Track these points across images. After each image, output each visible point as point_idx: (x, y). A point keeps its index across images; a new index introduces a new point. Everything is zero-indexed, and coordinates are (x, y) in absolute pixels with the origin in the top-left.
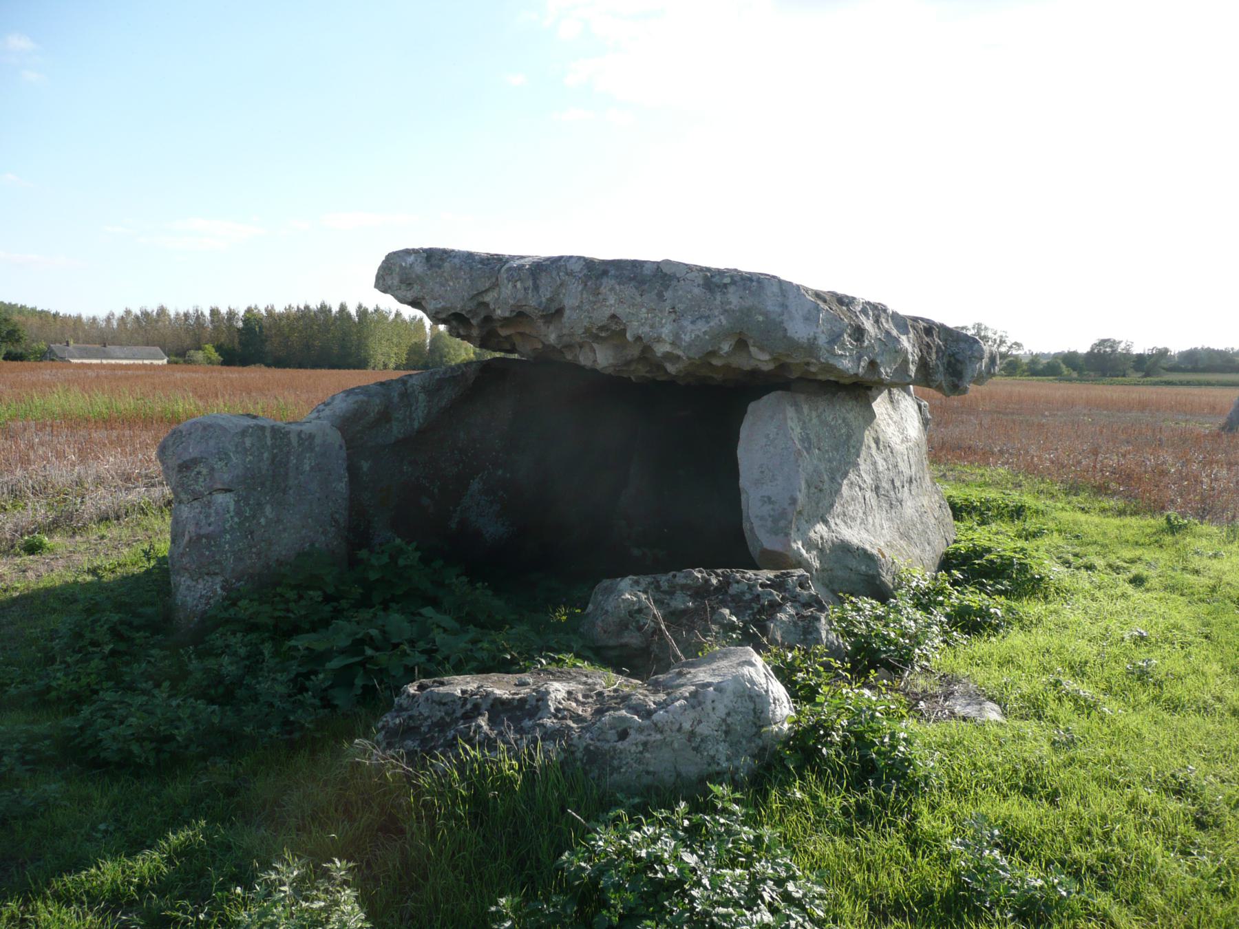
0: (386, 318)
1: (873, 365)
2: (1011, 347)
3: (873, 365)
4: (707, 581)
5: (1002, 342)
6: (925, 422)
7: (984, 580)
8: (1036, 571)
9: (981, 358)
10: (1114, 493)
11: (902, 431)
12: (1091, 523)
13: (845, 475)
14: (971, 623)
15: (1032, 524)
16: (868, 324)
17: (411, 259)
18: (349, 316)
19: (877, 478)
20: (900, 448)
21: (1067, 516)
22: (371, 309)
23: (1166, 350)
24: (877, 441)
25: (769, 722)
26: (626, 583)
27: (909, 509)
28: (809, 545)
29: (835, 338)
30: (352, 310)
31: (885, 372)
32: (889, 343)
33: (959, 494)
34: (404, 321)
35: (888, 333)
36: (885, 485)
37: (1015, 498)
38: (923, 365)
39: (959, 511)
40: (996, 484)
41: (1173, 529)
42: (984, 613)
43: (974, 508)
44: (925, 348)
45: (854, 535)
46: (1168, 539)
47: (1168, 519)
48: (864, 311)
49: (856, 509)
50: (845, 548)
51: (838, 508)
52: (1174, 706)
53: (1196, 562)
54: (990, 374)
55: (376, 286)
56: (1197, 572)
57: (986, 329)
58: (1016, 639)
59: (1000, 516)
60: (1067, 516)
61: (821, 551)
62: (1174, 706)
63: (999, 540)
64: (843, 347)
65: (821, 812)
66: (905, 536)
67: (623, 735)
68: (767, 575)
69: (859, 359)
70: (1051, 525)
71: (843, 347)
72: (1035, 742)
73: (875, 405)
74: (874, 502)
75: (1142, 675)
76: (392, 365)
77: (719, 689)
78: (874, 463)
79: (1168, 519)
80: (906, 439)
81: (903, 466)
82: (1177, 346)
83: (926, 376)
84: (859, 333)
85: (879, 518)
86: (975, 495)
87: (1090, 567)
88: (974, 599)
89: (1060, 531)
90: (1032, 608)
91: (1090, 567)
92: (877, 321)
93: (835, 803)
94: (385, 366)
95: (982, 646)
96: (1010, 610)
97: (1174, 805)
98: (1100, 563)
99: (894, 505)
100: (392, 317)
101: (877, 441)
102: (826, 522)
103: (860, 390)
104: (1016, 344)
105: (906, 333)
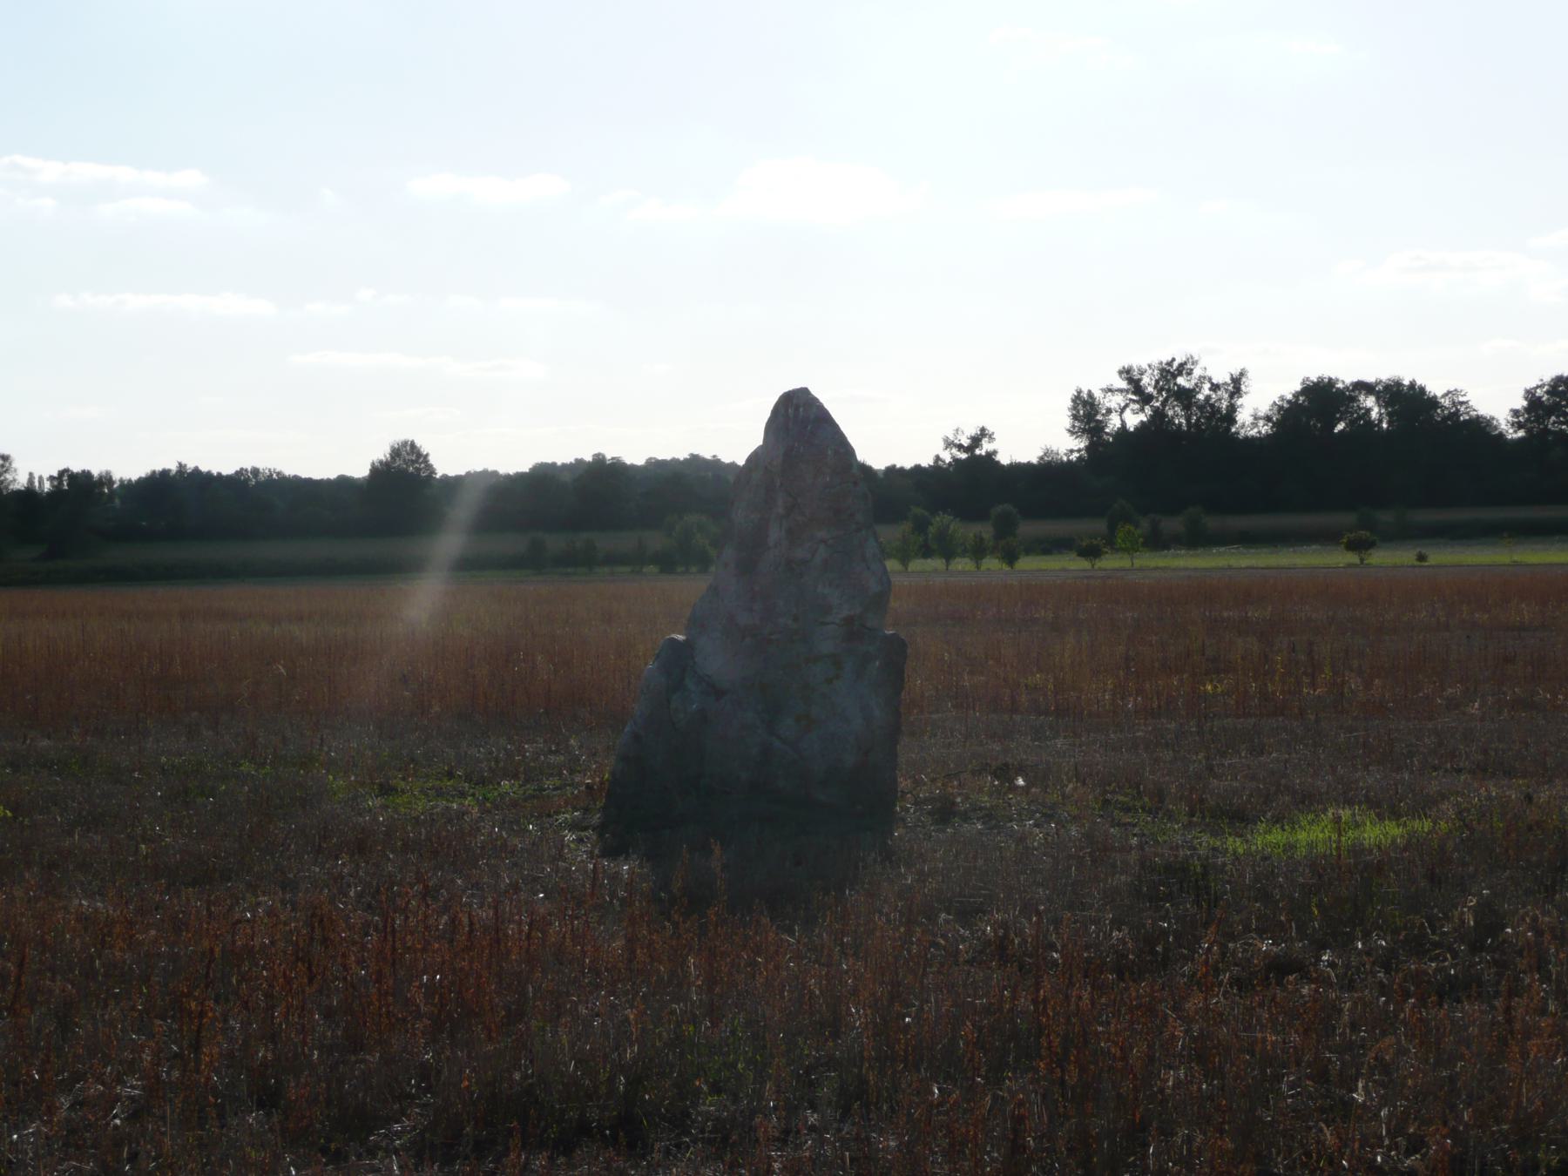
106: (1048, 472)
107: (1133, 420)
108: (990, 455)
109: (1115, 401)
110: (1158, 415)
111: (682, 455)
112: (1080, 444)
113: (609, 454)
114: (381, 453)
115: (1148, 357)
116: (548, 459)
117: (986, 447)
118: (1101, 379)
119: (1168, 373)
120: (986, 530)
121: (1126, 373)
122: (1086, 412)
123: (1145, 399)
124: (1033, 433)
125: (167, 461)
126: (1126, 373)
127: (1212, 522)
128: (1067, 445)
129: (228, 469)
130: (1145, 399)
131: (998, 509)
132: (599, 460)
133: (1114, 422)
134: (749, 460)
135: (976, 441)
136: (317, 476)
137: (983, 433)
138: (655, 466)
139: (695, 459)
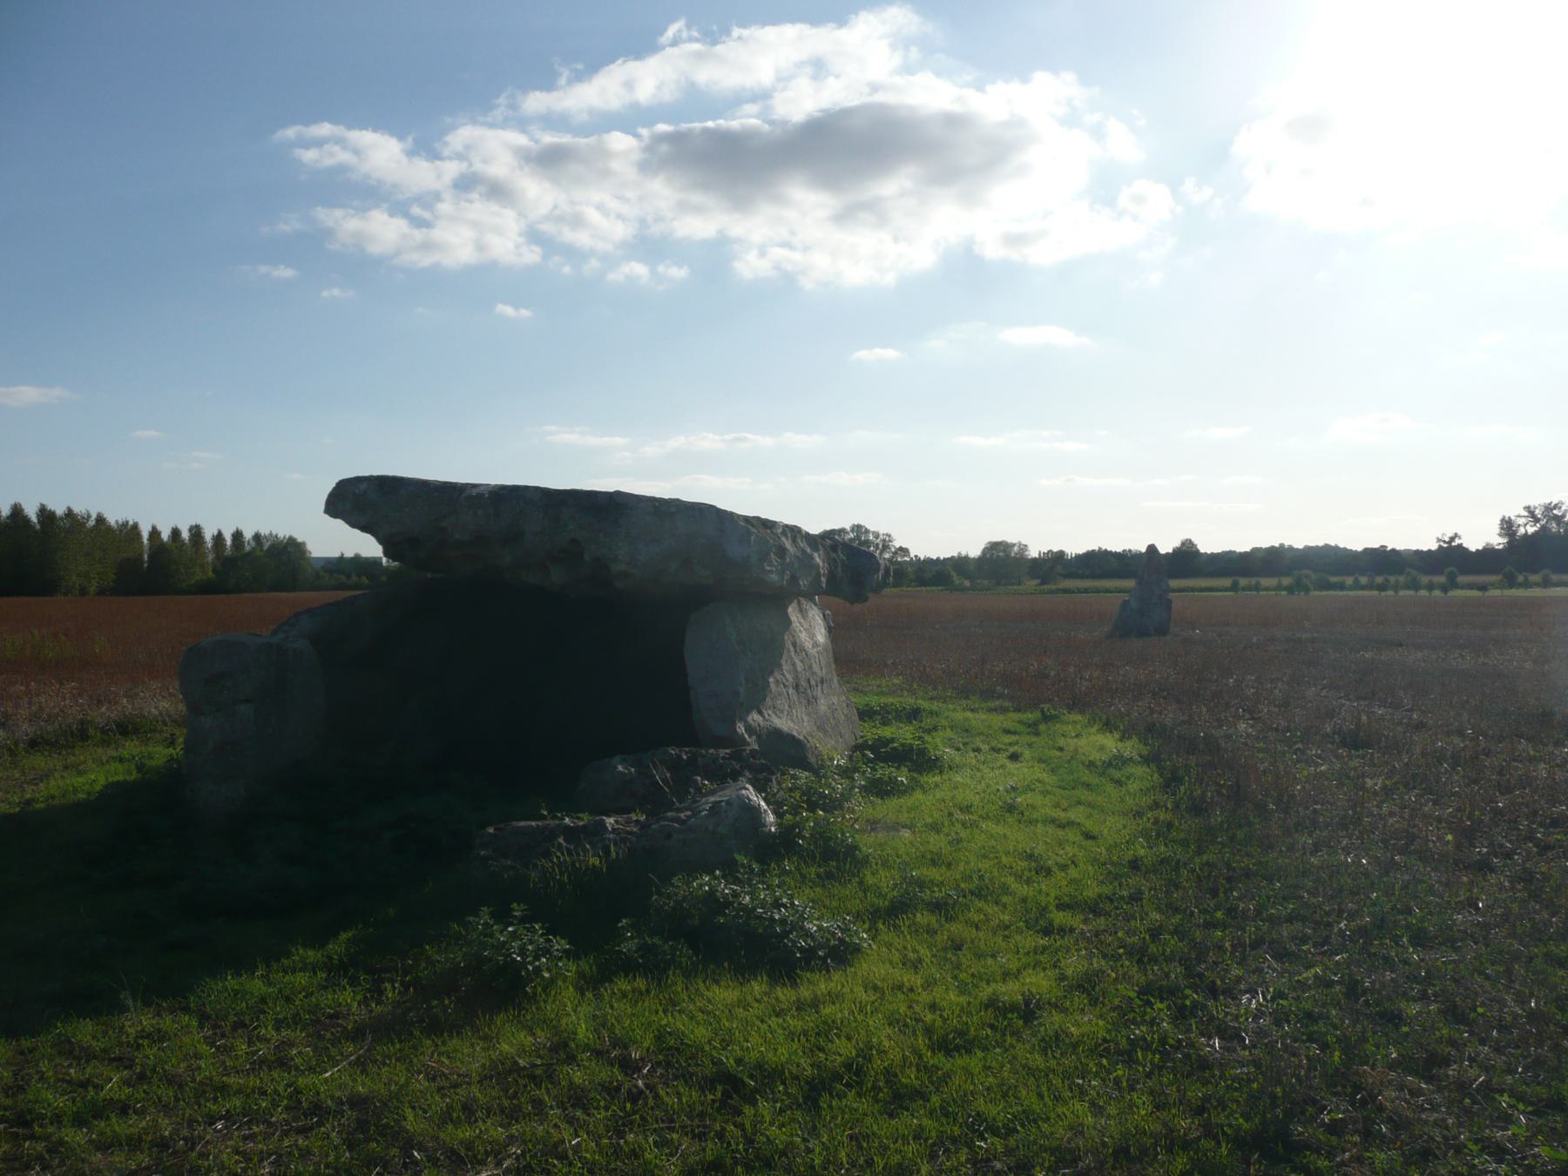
0: (83, 525)
1: (794, 579)
2: (895, 553)
3: (794, 579)
4: (679, 757)
5: (886, 547)
6: (830, 630)
7: (895, 761)
8: (932, 754)
9: (878, 570)
10: (1001, 696)
11: (812, 636)
12: (978, 719)
13: (771, 673)
14: (882, 789)
15: (928, 722)
16: (788, 544)
17: (364, 486)
18: (27, 520)
19: (796, 678)
20: (813, 652)
21: (959, 716)
22: (60, 511)
23: (1061, 553)
24: (794, 644)
25: (764, 825)
26: (617, 759)
27: (823, 706)
28: (749, 729)
29: (764, 557)
30: (31, 512)
31: (803, 583)
32: (806, 561)
33: (860, 700)
34: (109, 528)
35: (804, 551)
36: (804, 684)
37: (909, 701)
38: (832, 576)
39: (866, 714)
40: (892, 693)
41: (1047, 718)
42: (893, 781)
43: (876, 713)
44: (832, 562)
45: (783, 724)
46: (1042, 727)
47: (1043, 712)
48: (784, 533)
49: (782, 703)
50: (777, 734)
51: (769, 701)
52: (1031, 822)
53: (1061, 742)
54: (884, 584)
55: (326, 511)
56: (1061, 749)
57: (867, 531)
58: (918, 795)
59: (898, 718)
60: (959, 716)
61: (759, 737)
62: (1031, 822)
63: (903, 733)
64: (770, 564)
65: (803, 877)
66: (821, 728)
67: (669, 836)
68: (723, 752)
69: (783, 572)
70: (944, 722)
71: (770, 564)
72: (937, 842)
73: (790, 610)
74: (795, 697)
75: (1011, 808)
76: (92, 589)
77: (728, 803)
78: (794, 665)
79: (1043, 712)
80: (815, 645)
81: (816, 668)
82: (1075, 547)
83: (834, 587)
84: (782, 551)
85: (800, 711)
86: (874, 701)
87: (977, 750)
88: (884, 771)
89: (952, 728)
90: (931, 779)
91: (977, 750)
92: (794, 541)
93: (812, 871)
94: (83, 592)
95: (893, 802)
96: (912, 779)
97: (1024, 864)
98: (985, 747)
99: (811, 701)
100: (92, 523)
101: (794, 644)
102: (760, 713)
103: (777, 600)
104: (901, 549)
105: (817, 550)
106: (1488, 553)
107: (1531, 530)
108: (1460, 546)
109: (1521, 521)
110: (1543, 528)
111: (1321, 544)
112: (1505, 540)
113: (1287, 544)
114: (1177, 544)
115: (1538, 500)
116: (877, 523)
117: (1457, 542)
118: (1515, 511)
119: (1548, 508)
120: (1441, 579)
121: (1527, 508)
122: (1507, 526)
123: (1536, 520)
124: (1481, 535)
125: (1093, 546)
126: (1527, 508)
127: (1555, 578)
128: (1498, 541)
129: (1119, 550)
130: (1536, 520)
131: (1450, 569)
132: (303, 544)
133: (1522, 531)
134: (985, 551)
135: (1452, 539)
136: (1400, 547)
137: (1456, 535)
138: (1308, 549)
139: (1327, 546)
